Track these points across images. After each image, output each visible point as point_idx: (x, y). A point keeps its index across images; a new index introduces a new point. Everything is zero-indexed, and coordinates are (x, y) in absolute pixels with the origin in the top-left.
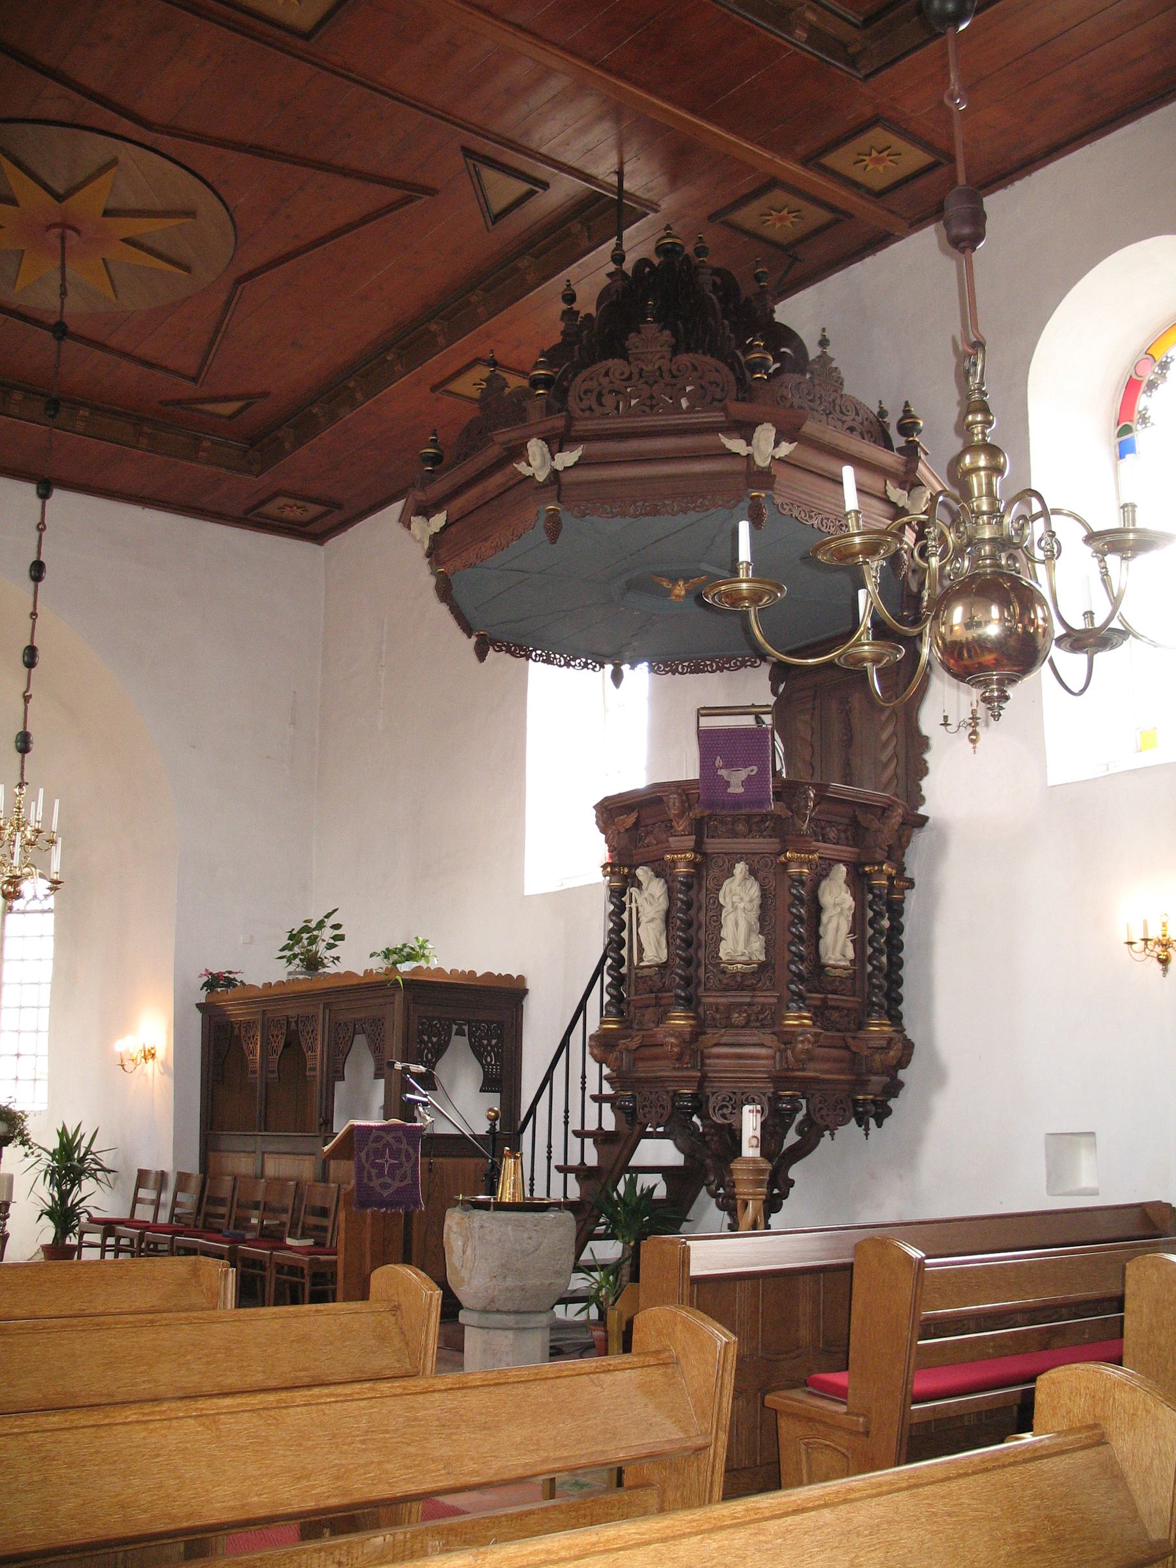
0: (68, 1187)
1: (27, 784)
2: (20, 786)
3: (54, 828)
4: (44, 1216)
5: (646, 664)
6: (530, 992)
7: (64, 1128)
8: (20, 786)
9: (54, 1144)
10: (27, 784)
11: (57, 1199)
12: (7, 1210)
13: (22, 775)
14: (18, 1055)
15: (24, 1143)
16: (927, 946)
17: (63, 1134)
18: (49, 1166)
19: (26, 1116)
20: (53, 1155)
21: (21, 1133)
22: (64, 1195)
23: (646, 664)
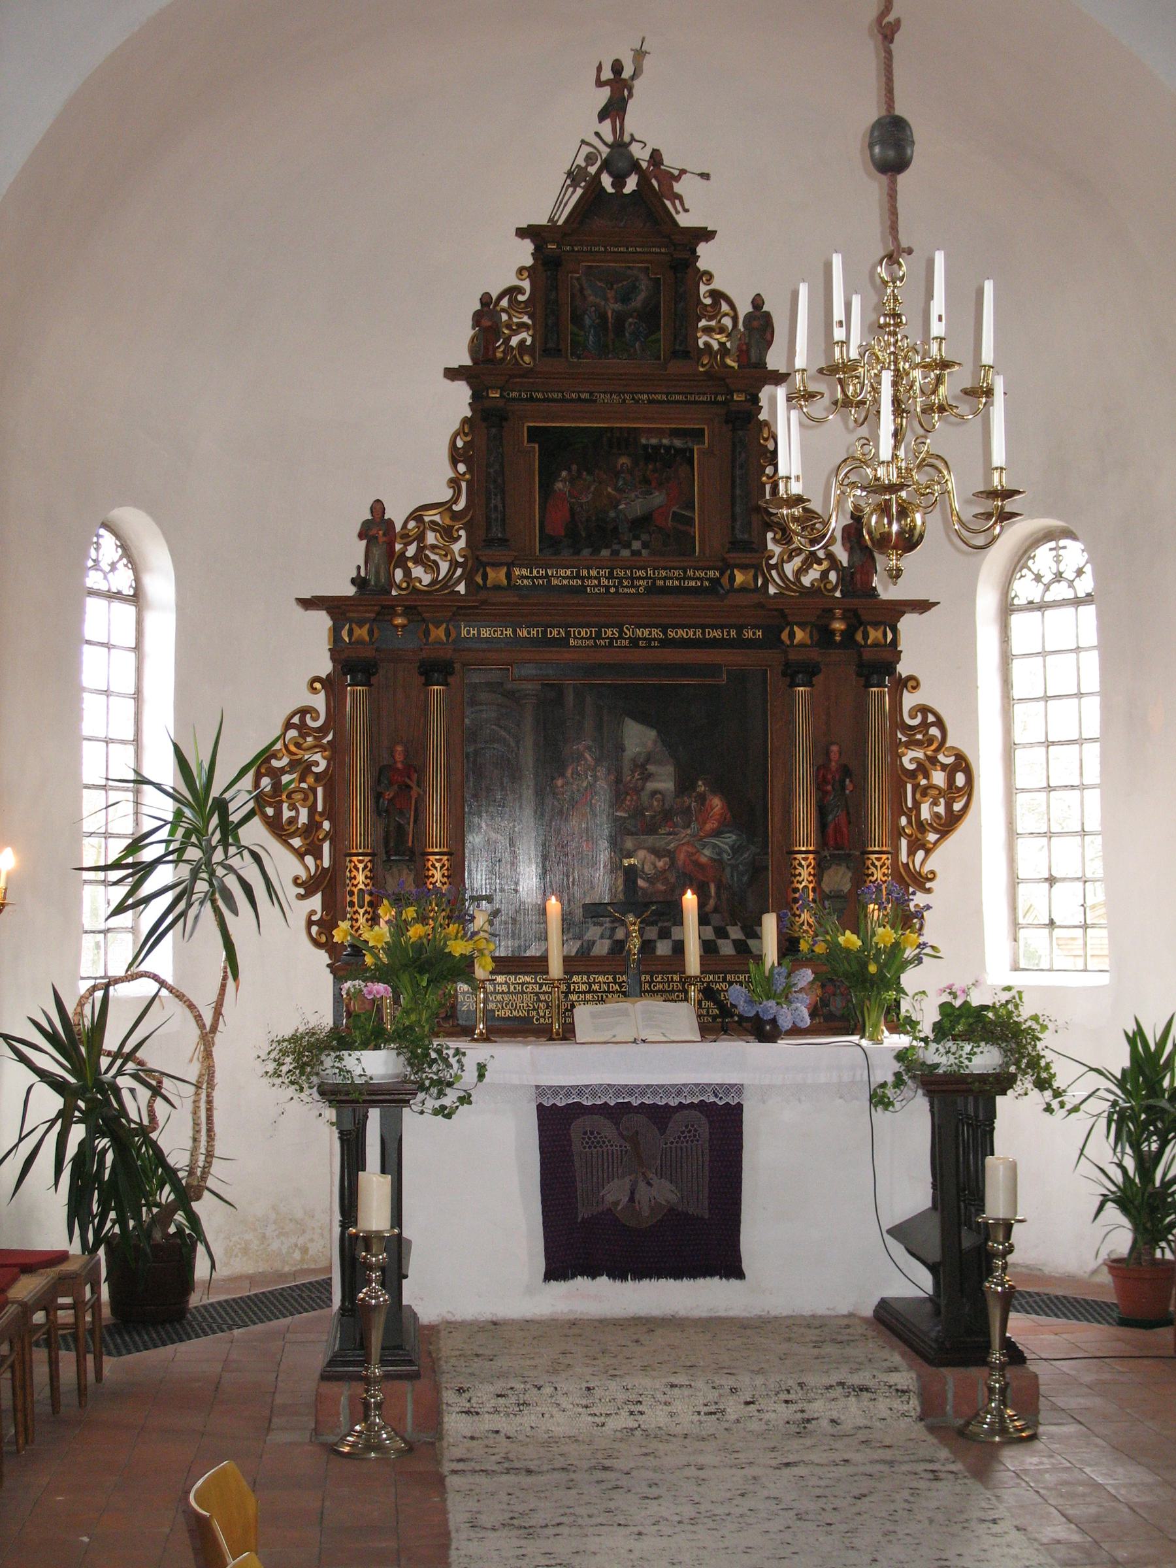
0: (1154, 1146)
1: (910, 251)
2: (892, 258)
3: (988, 356)
4: (1110, 1205)
5: (192, 1203)
6: (357, 528)
7: (1140, 1031)
8: (892, 258)
9: (1119, 1059)
10: (910, 251)
11: (1131, 1172)
12: (1008, 1236)
13: (894, 229)
14: (1051, 880)
15: (1042, 1084)
16: (329, 638)
17: (1136, 1038)
18: (1115, 1104)
19: (1044, 1028)
20: (1121, 1084)
21: (1034, 1063)
22: (1146, 1165)
23: (192, 1203)
